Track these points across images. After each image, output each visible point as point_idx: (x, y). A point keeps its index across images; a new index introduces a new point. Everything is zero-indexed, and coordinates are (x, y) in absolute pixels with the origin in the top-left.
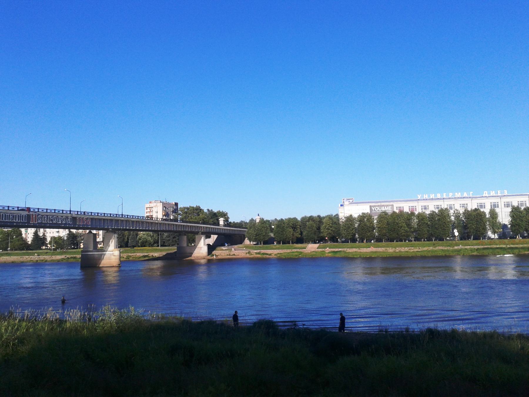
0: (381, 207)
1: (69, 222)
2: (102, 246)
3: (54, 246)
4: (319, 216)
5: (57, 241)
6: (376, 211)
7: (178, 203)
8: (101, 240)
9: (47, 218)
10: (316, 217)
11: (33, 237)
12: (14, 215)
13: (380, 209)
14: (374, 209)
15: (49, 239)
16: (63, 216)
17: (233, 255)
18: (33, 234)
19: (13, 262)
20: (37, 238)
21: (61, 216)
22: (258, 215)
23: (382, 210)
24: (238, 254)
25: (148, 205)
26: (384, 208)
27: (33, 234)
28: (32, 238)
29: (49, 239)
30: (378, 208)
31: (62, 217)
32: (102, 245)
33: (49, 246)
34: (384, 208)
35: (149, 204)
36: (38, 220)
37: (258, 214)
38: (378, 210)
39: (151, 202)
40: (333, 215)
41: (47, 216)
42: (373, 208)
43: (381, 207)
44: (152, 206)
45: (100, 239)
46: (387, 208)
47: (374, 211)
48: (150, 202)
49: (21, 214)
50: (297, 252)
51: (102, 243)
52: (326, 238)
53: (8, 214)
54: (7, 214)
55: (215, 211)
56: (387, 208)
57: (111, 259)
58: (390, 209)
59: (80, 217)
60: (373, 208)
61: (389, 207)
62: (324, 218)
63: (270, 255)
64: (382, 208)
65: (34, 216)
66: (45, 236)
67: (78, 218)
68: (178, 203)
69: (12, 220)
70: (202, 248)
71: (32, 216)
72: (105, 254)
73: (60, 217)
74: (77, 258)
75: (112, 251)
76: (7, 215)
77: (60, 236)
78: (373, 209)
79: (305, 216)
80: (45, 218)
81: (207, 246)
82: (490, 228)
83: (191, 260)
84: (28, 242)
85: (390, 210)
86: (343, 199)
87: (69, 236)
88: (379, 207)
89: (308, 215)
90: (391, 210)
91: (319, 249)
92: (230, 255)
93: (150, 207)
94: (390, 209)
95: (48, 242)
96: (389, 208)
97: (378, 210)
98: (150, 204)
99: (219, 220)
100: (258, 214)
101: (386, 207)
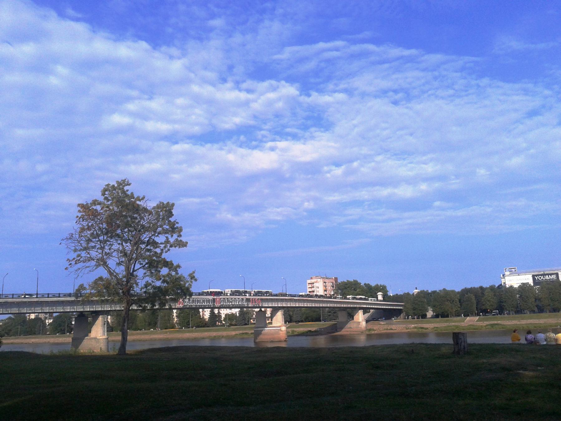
0: (545, 276)
1: (244, 303)
2: (270, 322)
3: (228, 323)
4: (481, 288)
5: (229, 317)
6: (540, 280)
7: (337, 278)
8: (269, 315)
9: (228, 301)
10: (477, 288)
11: (210, 315)
12: (203, 300)
13: (544, 278)
14: (538, 278)
15: (223, 316)
16: (239, 298)
17: (390, 330)
18: (210, 312)
19: (195, 338)
20: (213, 315)
21: (238, 298)
22: (415, 288)
23: (546, 279)
24: (395, 328)
25: (309, 281)
26: (549, 277)
27: (210, 312)
28: (209, 316)
29: (223, 316)
30: (542, 277)
31: (239, 298)
32: (270, 321)
33: (224, 322)
34: (549, 277)
35: (310, 280)
36: (221, 303)
37: (416, 288)
38: (542, 279)
39: (312, 278)
40: (497, 286)
41: (227, 298)
42: (537, 277)
43: (545, 276)
44: (313, 282)
45: (268, 315)
46: (551, 276)
47: (537, 280)
48: (312, 278)
49: (208, 298)
50: (453, 326)
51: (270, 319)
52: (489, 310)
53: (199, 299)
54: (198, 299)
55: (373, 284)
56: (551, 276)
57: (279, 334)
58: (555, 277)
59: (253, 298)
60: (537, 277)
61: (554, 275)
62: (486, 288)
63: (427, 329)
64: (546, 277)
65: (218, 300)
66: (221, 313)
67: (251, 299)
68: (337, 278)
69: (202, 304)
70: (361, 323)
71: (217, 299)
72: (263, 330)
73: (237, 299)
74: (249, 333)
75: (280, 327)
76: (199, 300)
77: (233, 313)
78: (537, 278)
79: (465, 288)
80: (226, 301)
81: (365, 321)
82: (101, 352)
83: (341, 336)
84: (206, 319)
85: (554, 278)
86: (505, 269)
87: (241, 313)
88: (543, 276)
89: (469, 286)
90: (556, 278)
91: (478, 322)
92: (387, 329)
93: (312, 282)
94: (555, 277)
95: (222, 319)
96: (554, 277)
97: (542, 279)
98: (311, 280)
99: (377, 294)
100: (416, 288)
101: (550, 276)
